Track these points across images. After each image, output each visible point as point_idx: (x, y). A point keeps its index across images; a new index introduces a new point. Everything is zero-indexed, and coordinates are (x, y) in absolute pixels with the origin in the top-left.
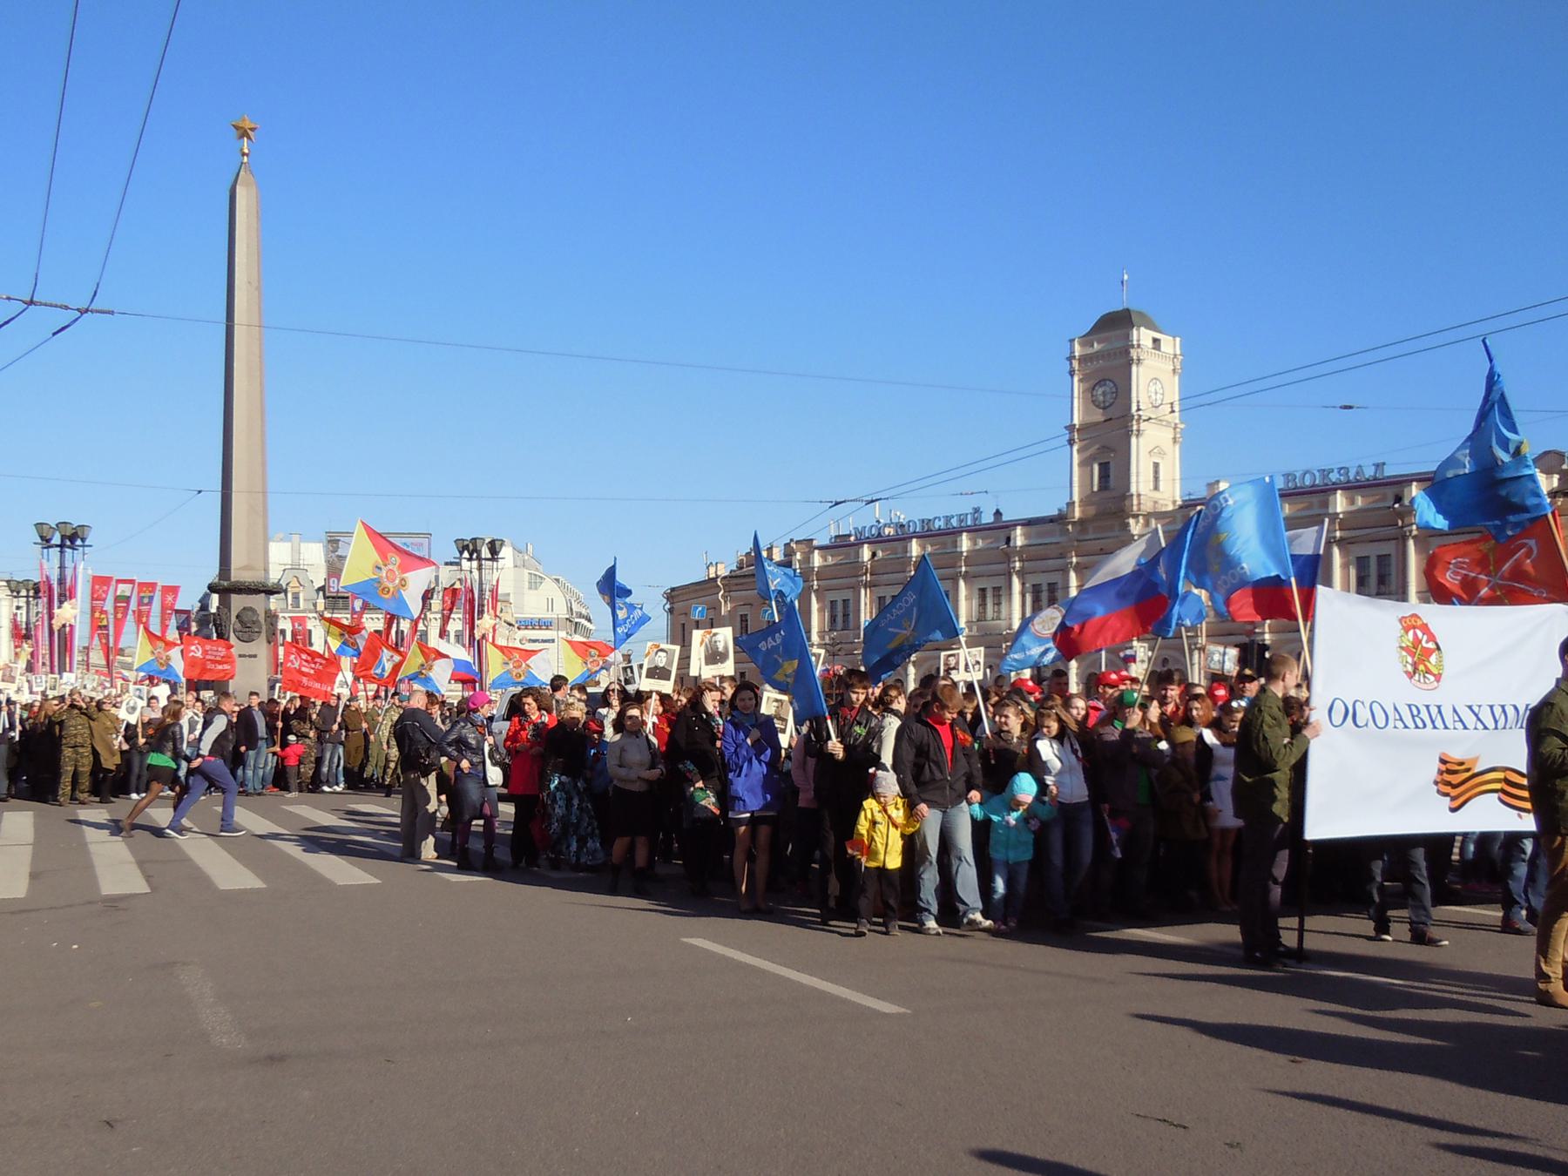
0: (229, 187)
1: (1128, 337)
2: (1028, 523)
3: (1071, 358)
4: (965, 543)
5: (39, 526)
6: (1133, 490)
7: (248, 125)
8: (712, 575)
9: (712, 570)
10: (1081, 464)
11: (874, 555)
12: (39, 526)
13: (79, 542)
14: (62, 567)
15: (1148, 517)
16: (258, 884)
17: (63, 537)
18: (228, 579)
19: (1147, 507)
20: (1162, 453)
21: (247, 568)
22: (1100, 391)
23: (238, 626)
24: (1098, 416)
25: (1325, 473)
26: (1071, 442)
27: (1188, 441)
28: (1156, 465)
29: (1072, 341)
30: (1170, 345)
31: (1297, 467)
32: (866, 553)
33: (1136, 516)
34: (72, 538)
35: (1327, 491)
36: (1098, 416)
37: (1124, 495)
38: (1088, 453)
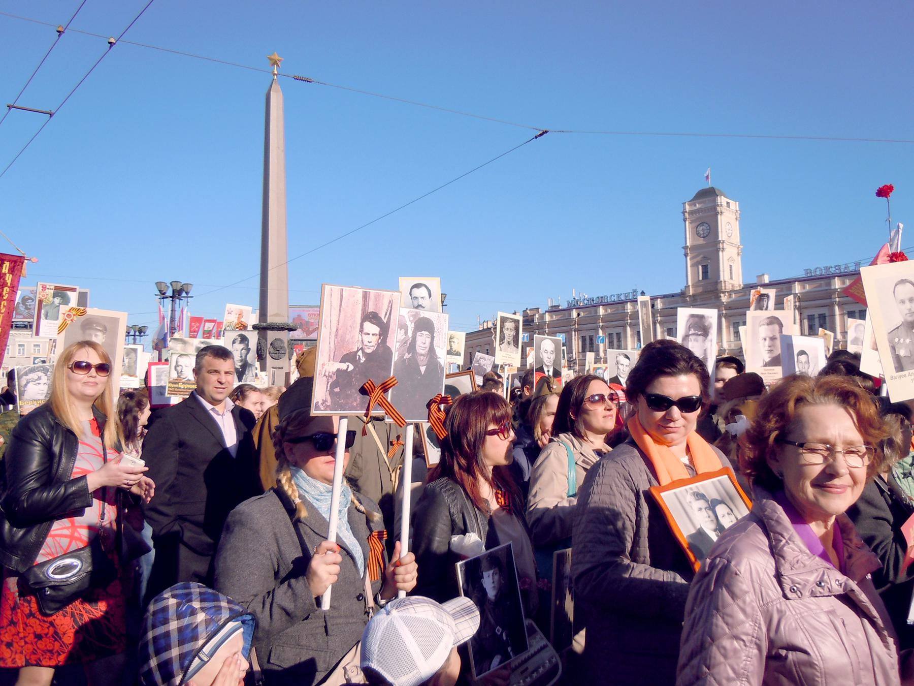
0: (266, 91)
1: (715, 201)
2: (664, 297)
3: (684, 213)
4: (601, 311)
5: (158, 284)
6: (722, 279)
7: (276, 57)
9: (485, 324)
10: (692, 266)
11: (579, 315)
12: (158, 284)
13: (184, 294)
14: (173, 311)
15: (730, 293)
16: (583, 633)
18: (265, 321)
19: (729, 287)
20: (733, 260)
21: (276, 315)
22: (701, 228)
23: (272, 350)
24: (701, 241)
25: (827, 268)
26: (686, 255)
27: (745, 253)
28: (731, 266)
29: (684, 204)
30: (734, 206)
31: (842, 263)
32: (574, 314)
33: (724, 292)
34: (178, 293)
35: (829, 278)
36: (701, 241)
37: (717, 282)
38: (695, 260)
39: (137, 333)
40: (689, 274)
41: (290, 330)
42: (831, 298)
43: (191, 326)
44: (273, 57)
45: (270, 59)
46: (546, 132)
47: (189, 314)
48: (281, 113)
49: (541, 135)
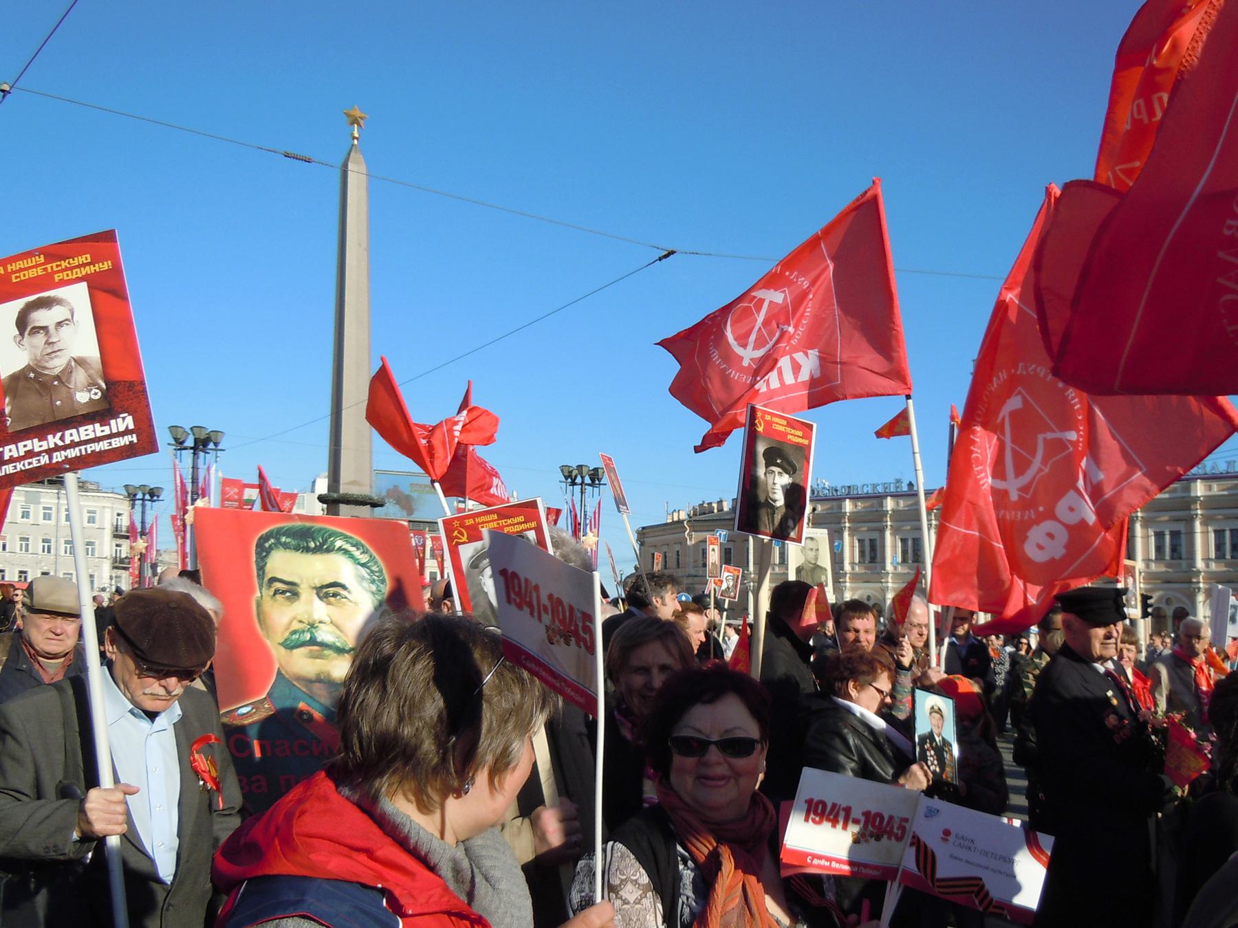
4: (889, 504)
7: (358, 113)
8: (676, 519)
9: (676, 515)
11: (814, 509)
13: (211, 446)
17: (196, 440)
21: (354, 483)
35: (881, 497)
39: (147, 497)
40: (919, 466)
41: (374, 505)
42: (1189, 509)
43: (223, 493)
44: (352, 113)
45: (348, 115)
46: (673, 252)
47: (220, 474)
48: (364, 194)
49: (666, 256)
